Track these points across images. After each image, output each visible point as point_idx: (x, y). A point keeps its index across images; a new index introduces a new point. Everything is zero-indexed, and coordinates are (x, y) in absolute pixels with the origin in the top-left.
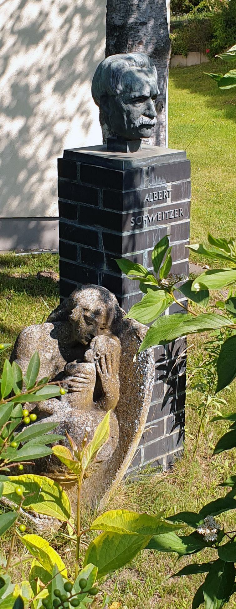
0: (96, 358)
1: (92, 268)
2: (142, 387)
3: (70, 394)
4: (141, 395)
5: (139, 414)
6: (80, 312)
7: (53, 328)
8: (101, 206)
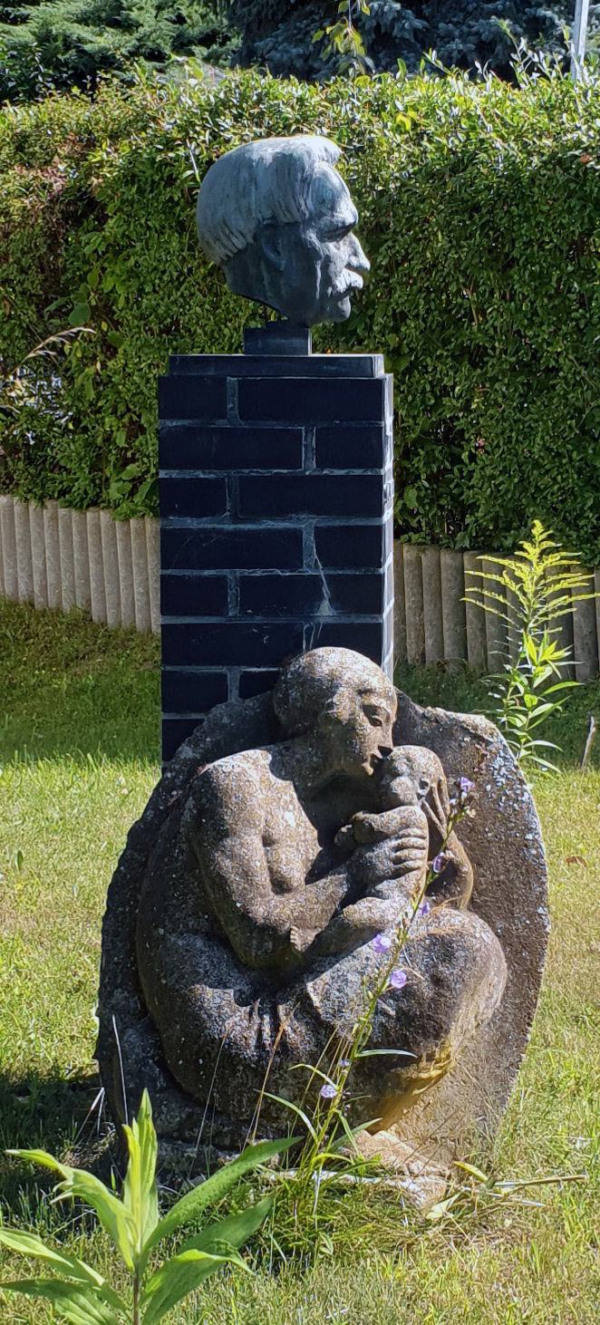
0: (420, 791)
1: (282, 620)
2: (529, 837)
3: (402, 879)
4: (534, 852)
5: (543, 893)
6: (352, 700)
7: (270, 757)
8: (310, 467)
